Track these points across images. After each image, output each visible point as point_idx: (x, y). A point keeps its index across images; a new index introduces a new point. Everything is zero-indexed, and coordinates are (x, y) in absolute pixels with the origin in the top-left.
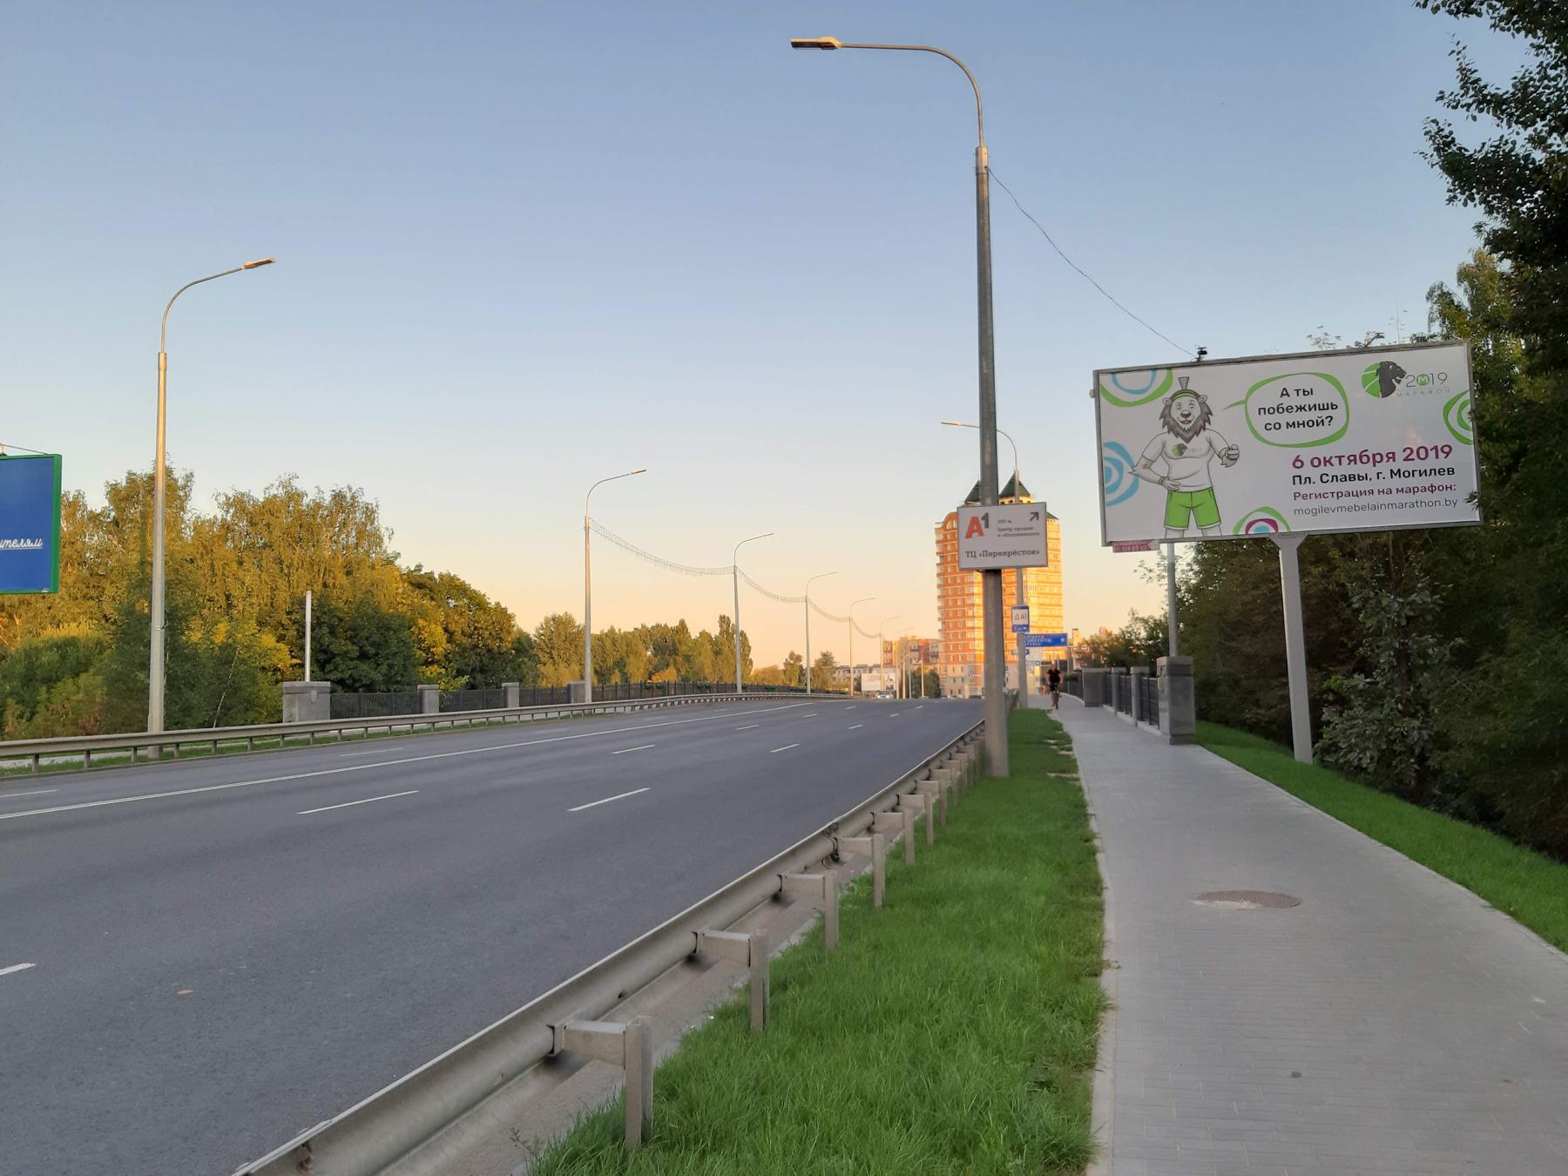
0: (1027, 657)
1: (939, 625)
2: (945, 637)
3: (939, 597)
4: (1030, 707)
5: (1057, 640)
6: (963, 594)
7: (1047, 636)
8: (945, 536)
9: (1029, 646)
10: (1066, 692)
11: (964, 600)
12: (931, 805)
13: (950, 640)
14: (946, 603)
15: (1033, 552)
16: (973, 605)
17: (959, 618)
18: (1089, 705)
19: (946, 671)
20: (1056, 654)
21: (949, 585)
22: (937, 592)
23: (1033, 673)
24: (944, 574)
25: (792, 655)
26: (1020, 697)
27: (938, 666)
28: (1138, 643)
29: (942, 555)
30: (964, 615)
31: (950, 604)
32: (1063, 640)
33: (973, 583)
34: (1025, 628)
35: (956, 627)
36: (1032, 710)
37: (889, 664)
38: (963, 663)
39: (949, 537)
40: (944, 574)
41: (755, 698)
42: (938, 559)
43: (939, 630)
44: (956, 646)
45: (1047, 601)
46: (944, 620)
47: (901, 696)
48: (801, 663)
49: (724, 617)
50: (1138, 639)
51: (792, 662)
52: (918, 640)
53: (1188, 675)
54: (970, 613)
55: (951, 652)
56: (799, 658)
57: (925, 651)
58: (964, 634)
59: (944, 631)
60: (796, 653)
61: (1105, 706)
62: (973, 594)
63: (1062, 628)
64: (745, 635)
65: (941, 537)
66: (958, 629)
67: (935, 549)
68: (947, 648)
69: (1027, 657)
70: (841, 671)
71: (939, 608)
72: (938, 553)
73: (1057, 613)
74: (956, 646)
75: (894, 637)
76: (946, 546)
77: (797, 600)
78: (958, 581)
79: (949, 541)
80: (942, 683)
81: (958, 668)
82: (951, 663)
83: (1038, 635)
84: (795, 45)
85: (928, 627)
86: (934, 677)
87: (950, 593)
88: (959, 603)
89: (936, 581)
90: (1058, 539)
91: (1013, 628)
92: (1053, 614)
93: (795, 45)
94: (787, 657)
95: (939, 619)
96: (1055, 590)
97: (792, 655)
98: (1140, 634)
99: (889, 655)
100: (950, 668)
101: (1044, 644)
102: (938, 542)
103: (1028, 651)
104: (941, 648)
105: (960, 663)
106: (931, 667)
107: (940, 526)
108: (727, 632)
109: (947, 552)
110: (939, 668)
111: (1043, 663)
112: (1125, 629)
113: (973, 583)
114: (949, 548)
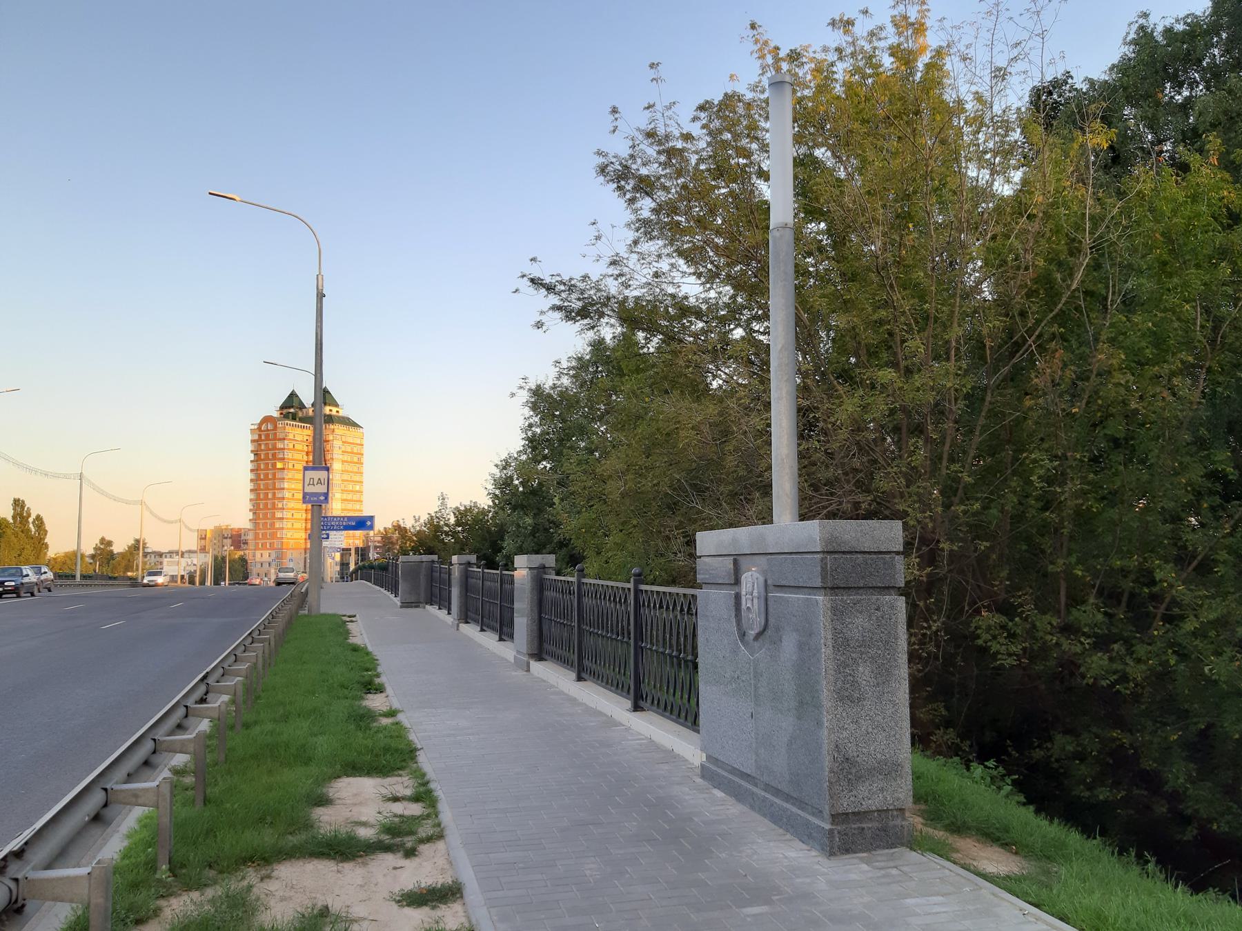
0: (325, 543)
1: (251, 516)
2: (255, 527)
3: (251, 490)
4: (323, 611)
5: (362, 523)
6: (274, 488)
7: (350, 518)
8: (260, 436)
9: (329, 530)
10: (370, 582)
11: (274, 494)
12: (197, 731)
13: (260, 529)
14: (258, 498)
15: (321, 296)
16: (283, 498)
17: (269, 509)
18: (406, 605)
19: (254, 556)
20: (355, 539)
21: (261, 480)
22: (250, 486)
23: (333, 559)
24: (257, 470)
25: (102, 540)
26: (310, 598)
27: (247, 552)
28: (446, 529)
29: (256, 453)
30: (274, 507)
31: (262, 496)
32: (369, 523)
33: (284, 479)
34: (322, 498)
35: (265, 517)
36: (324, 615)
37: (203, 550)
38: (270, 549)
39: (263, 438)
40: (257, 470)
41: (61, 586)
42: (252, 457)
43: (250, 520)
44: (264, 535)
45: (349, 497)
46: (255, 510)
47: (203, 582)
48: (112, 548)
49: (19, 500)
50: (447, 525)
51: (102, 547)
52: (232, 529)
53: (887, 589)
54: (280, 506)
55: (260, 539)
56: (110, 543)
57: (237, 539)
58: (273, 524)
59: (254, 521)
60: (107, 538)
61: (428, 607)
62: (283, 489)
63: (362, 511)
64: (41, 519)
65: (256, 437)
66: (268, 519)
67: (250, 447)
68: (256, 536)
69: (325, 543)
70: (153, 556)
71: (251, 500)
72: (252, 451)
73: (358, 508)
74: (264, 535)
75: (209, 526)
76: (260, 445)
77: (66, 477)
78: (270, 477)
79: (264, 440)
80: (249, 568)
81: (266, 553)
82: (259, 549)
83: (340, 517)
84: (210, 194)
85: (240, 517)
86: (243, 561)
87: (262, 487)
88: (270, 496)
89: (250, 476)
90: (362, 445)
91: (304, 497)
92: (354, 499)
93: (210, 194)
94: (98, 542)
95: (250, 510)
96: (357, 488)
97: (102, 540)
98: (449, 519)
99: (203, 541)
100: (258, 553)
101: (347, 528)
102: (253, 441)
103: (328, 535)
104: (250, 537)
105: (268, 549)
106: (241, 553)
107: (256, 427)
108: (21, 515)
109: (262, 450)
110: (249, 554)
111: (343, 550)
112: (433, 515)
113: (284, 479)
114: (263, 447)
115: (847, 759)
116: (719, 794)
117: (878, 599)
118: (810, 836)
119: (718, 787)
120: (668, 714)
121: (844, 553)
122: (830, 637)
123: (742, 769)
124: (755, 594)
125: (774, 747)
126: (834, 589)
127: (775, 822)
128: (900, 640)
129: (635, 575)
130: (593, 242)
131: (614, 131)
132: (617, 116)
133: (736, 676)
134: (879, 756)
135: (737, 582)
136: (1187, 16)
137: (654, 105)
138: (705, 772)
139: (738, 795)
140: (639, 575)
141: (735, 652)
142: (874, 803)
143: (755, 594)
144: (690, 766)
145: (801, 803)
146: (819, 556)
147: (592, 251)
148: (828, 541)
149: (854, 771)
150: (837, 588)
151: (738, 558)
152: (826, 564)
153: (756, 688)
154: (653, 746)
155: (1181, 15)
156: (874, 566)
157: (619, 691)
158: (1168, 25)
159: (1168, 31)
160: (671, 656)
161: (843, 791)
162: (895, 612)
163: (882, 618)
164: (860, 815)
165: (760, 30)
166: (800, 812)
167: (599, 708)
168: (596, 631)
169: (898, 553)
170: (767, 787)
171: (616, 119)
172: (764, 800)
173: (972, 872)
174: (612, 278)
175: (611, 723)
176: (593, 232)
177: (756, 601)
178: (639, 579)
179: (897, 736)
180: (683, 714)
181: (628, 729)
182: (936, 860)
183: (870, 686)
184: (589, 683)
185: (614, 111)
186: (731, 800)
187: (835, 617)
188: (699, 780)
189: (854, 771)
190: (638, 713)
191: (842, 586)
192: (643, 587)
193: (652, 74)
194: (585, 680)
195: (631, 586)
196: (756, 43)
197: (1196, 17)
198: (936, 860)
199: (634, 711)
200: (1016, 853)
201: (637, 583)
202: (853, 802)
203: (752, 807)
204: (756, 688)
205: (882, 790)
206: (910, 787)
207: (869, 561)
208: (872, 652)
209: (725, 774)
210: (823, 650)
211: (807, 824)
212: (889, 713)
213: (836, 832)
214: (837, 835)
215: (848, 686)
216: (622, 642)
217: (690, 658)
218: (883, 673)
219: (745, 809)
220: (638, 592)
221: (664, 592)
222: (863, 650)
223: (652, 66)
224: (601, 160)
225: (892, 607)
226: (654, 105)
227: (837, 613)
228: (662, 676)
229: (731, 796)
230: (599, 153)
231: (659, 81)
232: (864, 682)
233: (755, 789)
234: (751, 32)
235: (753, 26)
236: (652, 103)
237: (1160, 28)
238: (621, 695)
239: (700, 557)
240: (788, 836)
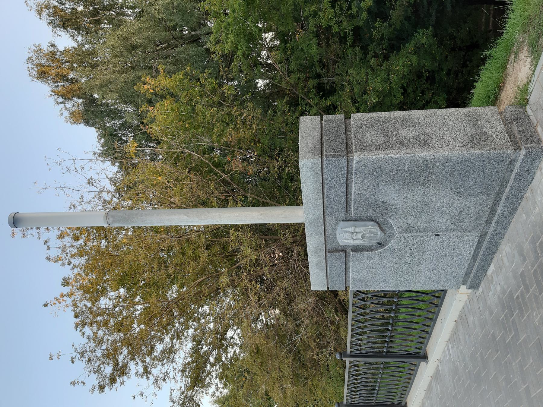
53: (347, 126)
115: (470, 141)
116: (492, 269)
117: (354, 127)
118: (529, 171)
119: (485, 271)
120: (408, 389)
121: (322, 147)
122: (382, 152)
123: (474, 247)
124: (352, 229)
125: (461, 212)
126: (348, 151)
127: (515, 212)
128: (381, 116)
129: (341, 357)
130: (144, 397)
131: (84, 383)
132: (76, 382)
133: (409, 251)
134: (464, 124)
135: (344, 250)
136: (98, 138)
137: (72, 357)
138: (474, 286)
139: (493, 249)
140: (341, 354)
141: (392, 251)
142: (501, 128)
143: (352, 229)
144: (468, 303)
145: (504, 183)
146: (325, 159)
147: (150, 398)
148: (313, 153)
149: (478, 137)
150: (347, 150)
151: (327, 250)
152: (330, 155)
153: (418, 231)
154: (454, 337)
155: (97, 140)
156: (331, 130)
157: (411, 381)
158: (100, 146)
159: (103, 146)
160: (381, 378)
161: (495, 143)
162: (362, 118)
163: (366, 125)
164: (510, 134)
165: (49, 302)
166: (509, 185)
167: (426, 389)
168: (376, 392)
169: (322, 119)
170: (489, 222)
171: (78, 382)
172: (498, 223)
173: (536, 68)
174: (173, 393)
175: (437, 376)
176: (138, 398)
177: (357, 230)
178: (343, 354)
179: (448, 115)
180: (402, 396)
181: (440, 361)
182: (535, 79)
183: (415, 130)
184: (408, 400)
185: (73, 383)
186: (497, 257)
187: (368, 149)
188: (480, 289)
189: (478, 137)
190: (429, 356)
191: (345, 146)
192: (348, 350)
193: (55, 358)
194: (406, 403)
195: (347, 360)
196: (55, 304)
197: (99, 135)
198: (535, 79)
199: (427, 359)
200: (504, 83)
201: (346, 356)
202: (501, 137)
203: (502, 236)
204: (418, 231)
205: (488, 122)
206: (482, 108)
207: (328, 132)
208: (390, 129)
209: (477, 264)
210: (393, 155)
211: (519, 174)
212: (432, 120)
213: (527, 146)
214: (528, 145)
215: (417, 142)
216: (379, 387)
217: (382, 366)
218: (405, 124)
219: (504, 241)
220: (351, 356)
221: (352, 331)
222: (390, 134)
223: (51, 359)
224: (96, 390)
225: (359, 120)
226: (72, 357)
227: (364, 148)
228: (406, 335)
229: (493, 258)
230: (92, 391)
231: (60, 354)
232: (413, 133)
233: (490, 233)
234: (49, 306)
235: (46, 305)
236: (70, 359)
237: (102, 149)
238: (413, 380)
239: (328, 288)
240: (528, 194)
